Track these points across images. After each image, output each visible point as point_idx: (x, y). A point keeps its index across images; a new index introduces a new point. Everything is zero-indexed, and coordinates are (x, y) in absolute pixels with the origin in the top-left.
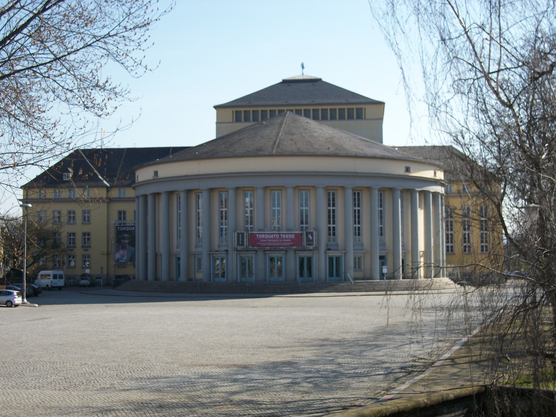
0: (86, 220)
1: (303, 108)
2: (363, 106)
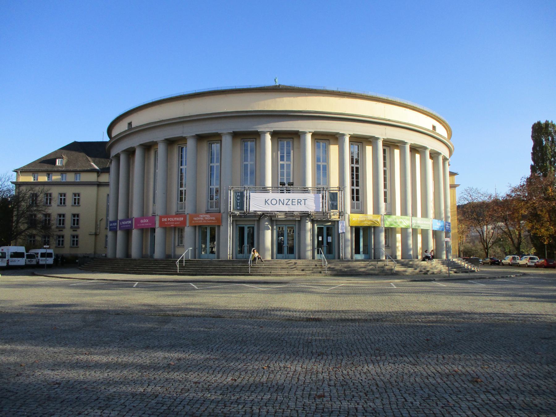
0: (77, 202)
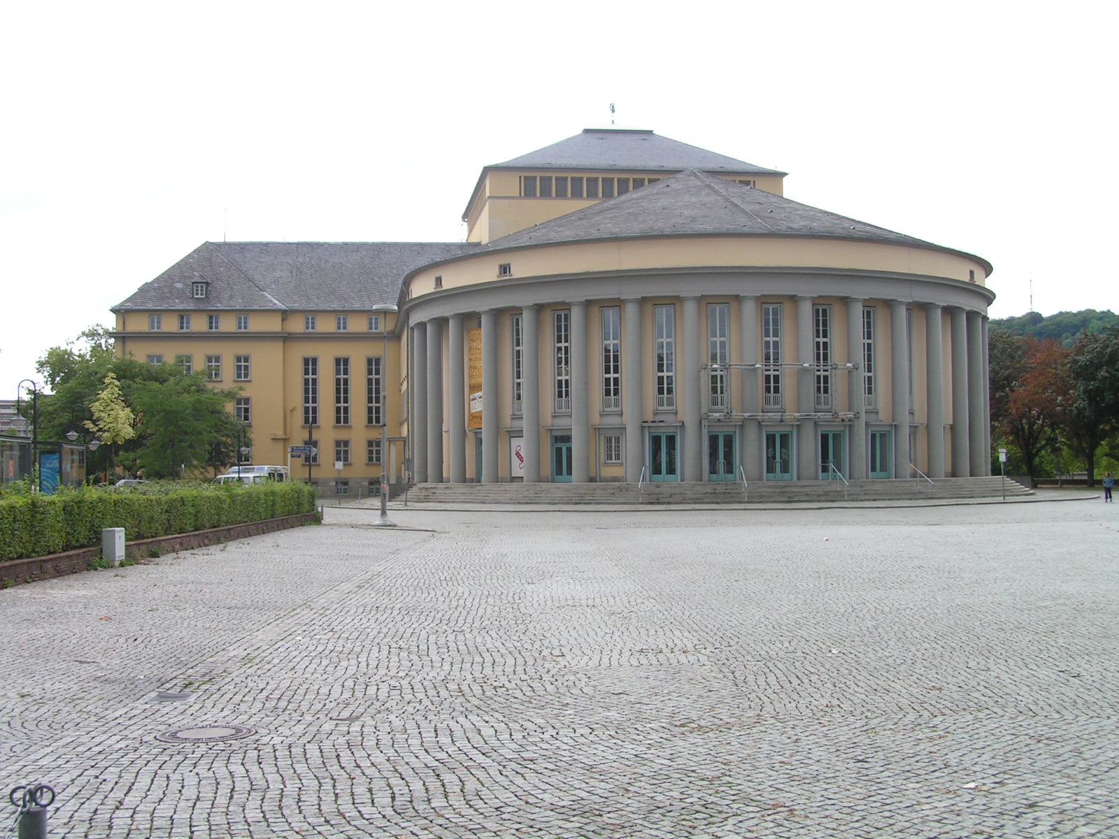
0: (243, 368)
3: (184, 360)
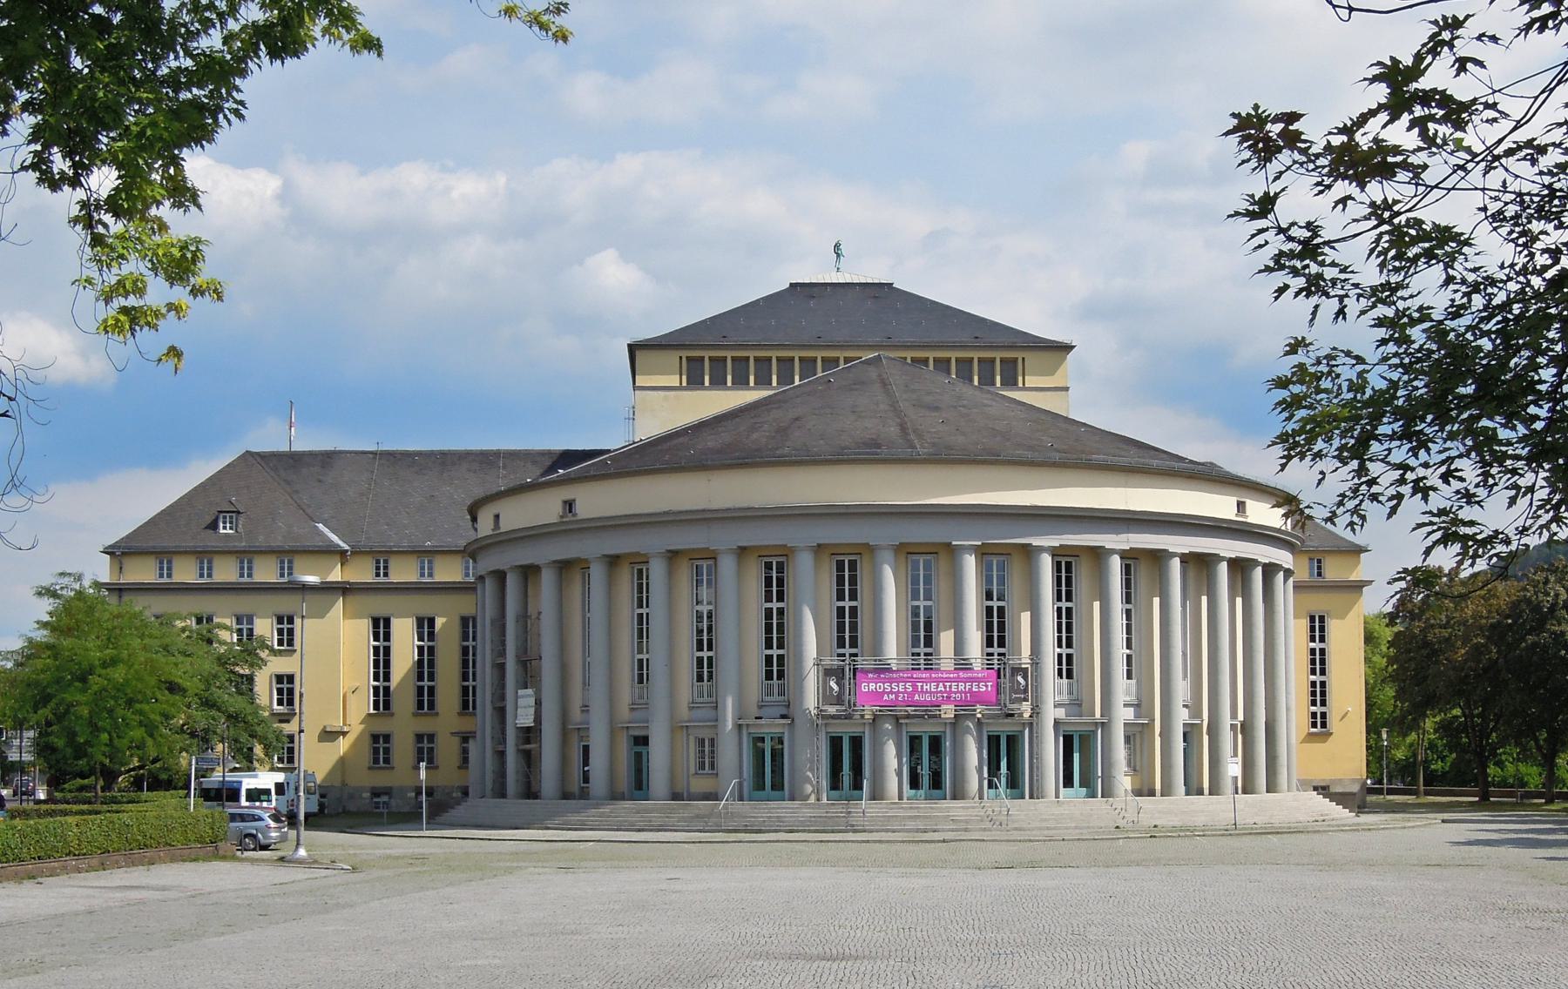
1: (953, 355)
2: (1019, 355)
3: (164, 620)
